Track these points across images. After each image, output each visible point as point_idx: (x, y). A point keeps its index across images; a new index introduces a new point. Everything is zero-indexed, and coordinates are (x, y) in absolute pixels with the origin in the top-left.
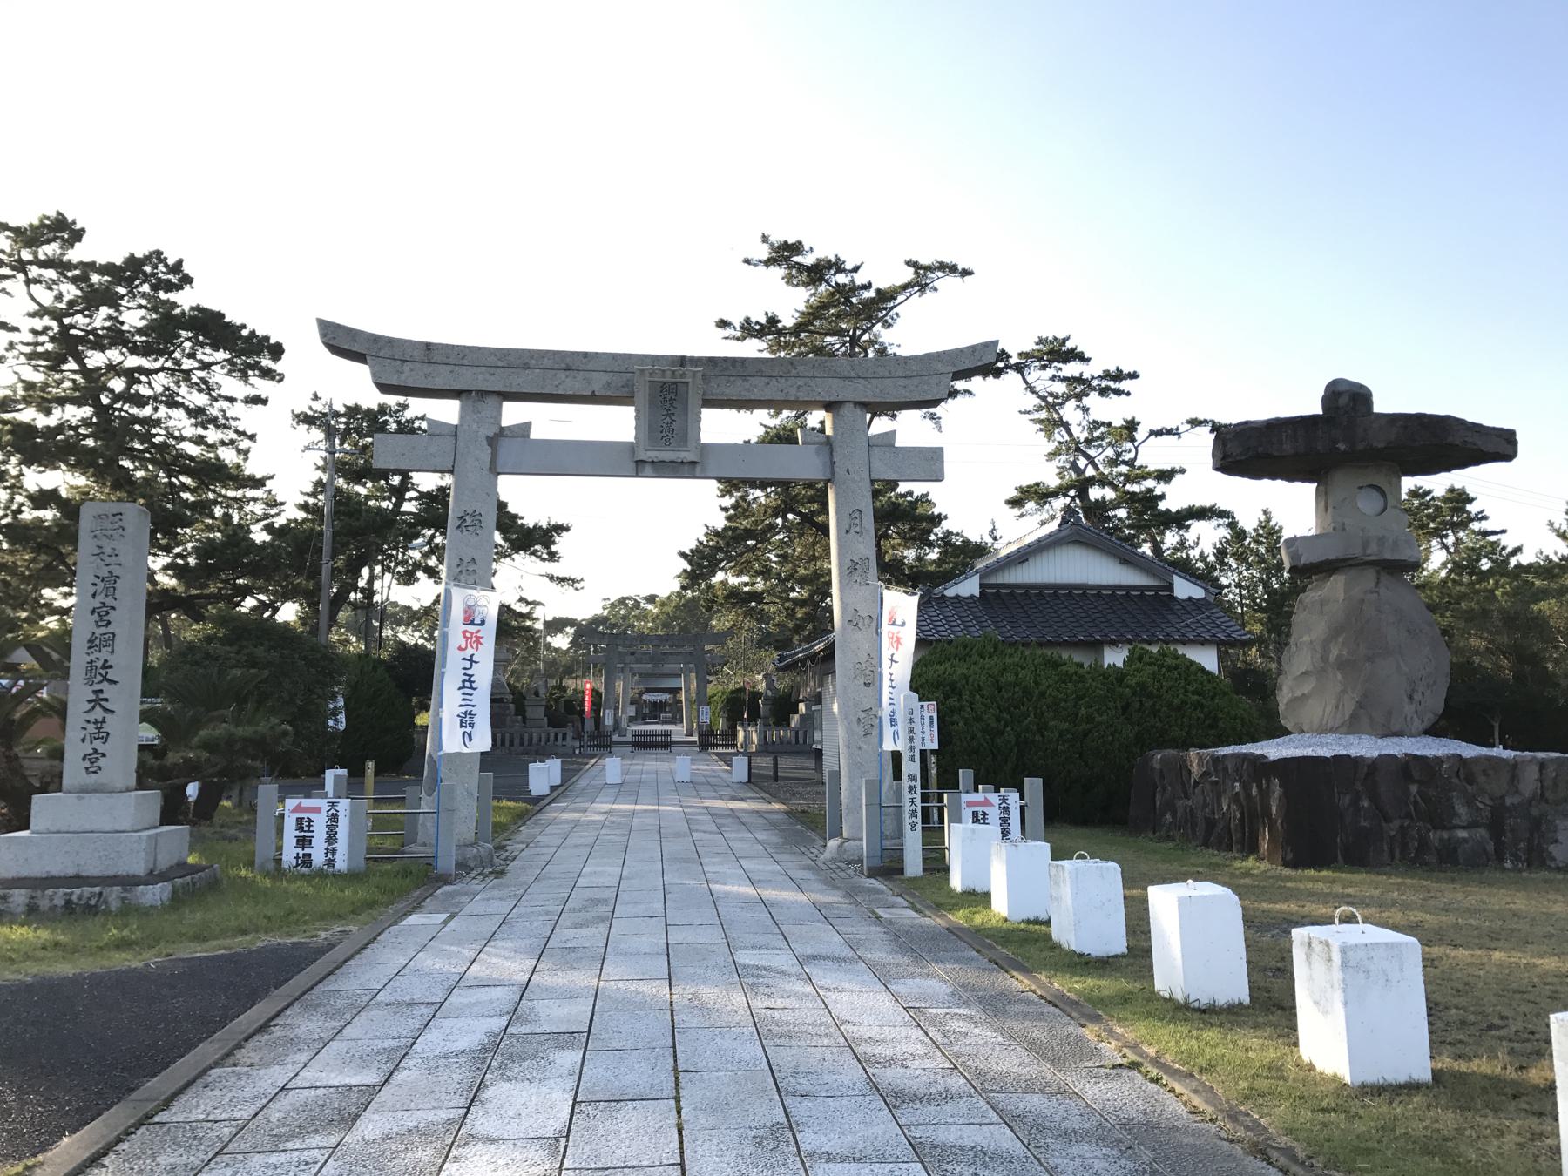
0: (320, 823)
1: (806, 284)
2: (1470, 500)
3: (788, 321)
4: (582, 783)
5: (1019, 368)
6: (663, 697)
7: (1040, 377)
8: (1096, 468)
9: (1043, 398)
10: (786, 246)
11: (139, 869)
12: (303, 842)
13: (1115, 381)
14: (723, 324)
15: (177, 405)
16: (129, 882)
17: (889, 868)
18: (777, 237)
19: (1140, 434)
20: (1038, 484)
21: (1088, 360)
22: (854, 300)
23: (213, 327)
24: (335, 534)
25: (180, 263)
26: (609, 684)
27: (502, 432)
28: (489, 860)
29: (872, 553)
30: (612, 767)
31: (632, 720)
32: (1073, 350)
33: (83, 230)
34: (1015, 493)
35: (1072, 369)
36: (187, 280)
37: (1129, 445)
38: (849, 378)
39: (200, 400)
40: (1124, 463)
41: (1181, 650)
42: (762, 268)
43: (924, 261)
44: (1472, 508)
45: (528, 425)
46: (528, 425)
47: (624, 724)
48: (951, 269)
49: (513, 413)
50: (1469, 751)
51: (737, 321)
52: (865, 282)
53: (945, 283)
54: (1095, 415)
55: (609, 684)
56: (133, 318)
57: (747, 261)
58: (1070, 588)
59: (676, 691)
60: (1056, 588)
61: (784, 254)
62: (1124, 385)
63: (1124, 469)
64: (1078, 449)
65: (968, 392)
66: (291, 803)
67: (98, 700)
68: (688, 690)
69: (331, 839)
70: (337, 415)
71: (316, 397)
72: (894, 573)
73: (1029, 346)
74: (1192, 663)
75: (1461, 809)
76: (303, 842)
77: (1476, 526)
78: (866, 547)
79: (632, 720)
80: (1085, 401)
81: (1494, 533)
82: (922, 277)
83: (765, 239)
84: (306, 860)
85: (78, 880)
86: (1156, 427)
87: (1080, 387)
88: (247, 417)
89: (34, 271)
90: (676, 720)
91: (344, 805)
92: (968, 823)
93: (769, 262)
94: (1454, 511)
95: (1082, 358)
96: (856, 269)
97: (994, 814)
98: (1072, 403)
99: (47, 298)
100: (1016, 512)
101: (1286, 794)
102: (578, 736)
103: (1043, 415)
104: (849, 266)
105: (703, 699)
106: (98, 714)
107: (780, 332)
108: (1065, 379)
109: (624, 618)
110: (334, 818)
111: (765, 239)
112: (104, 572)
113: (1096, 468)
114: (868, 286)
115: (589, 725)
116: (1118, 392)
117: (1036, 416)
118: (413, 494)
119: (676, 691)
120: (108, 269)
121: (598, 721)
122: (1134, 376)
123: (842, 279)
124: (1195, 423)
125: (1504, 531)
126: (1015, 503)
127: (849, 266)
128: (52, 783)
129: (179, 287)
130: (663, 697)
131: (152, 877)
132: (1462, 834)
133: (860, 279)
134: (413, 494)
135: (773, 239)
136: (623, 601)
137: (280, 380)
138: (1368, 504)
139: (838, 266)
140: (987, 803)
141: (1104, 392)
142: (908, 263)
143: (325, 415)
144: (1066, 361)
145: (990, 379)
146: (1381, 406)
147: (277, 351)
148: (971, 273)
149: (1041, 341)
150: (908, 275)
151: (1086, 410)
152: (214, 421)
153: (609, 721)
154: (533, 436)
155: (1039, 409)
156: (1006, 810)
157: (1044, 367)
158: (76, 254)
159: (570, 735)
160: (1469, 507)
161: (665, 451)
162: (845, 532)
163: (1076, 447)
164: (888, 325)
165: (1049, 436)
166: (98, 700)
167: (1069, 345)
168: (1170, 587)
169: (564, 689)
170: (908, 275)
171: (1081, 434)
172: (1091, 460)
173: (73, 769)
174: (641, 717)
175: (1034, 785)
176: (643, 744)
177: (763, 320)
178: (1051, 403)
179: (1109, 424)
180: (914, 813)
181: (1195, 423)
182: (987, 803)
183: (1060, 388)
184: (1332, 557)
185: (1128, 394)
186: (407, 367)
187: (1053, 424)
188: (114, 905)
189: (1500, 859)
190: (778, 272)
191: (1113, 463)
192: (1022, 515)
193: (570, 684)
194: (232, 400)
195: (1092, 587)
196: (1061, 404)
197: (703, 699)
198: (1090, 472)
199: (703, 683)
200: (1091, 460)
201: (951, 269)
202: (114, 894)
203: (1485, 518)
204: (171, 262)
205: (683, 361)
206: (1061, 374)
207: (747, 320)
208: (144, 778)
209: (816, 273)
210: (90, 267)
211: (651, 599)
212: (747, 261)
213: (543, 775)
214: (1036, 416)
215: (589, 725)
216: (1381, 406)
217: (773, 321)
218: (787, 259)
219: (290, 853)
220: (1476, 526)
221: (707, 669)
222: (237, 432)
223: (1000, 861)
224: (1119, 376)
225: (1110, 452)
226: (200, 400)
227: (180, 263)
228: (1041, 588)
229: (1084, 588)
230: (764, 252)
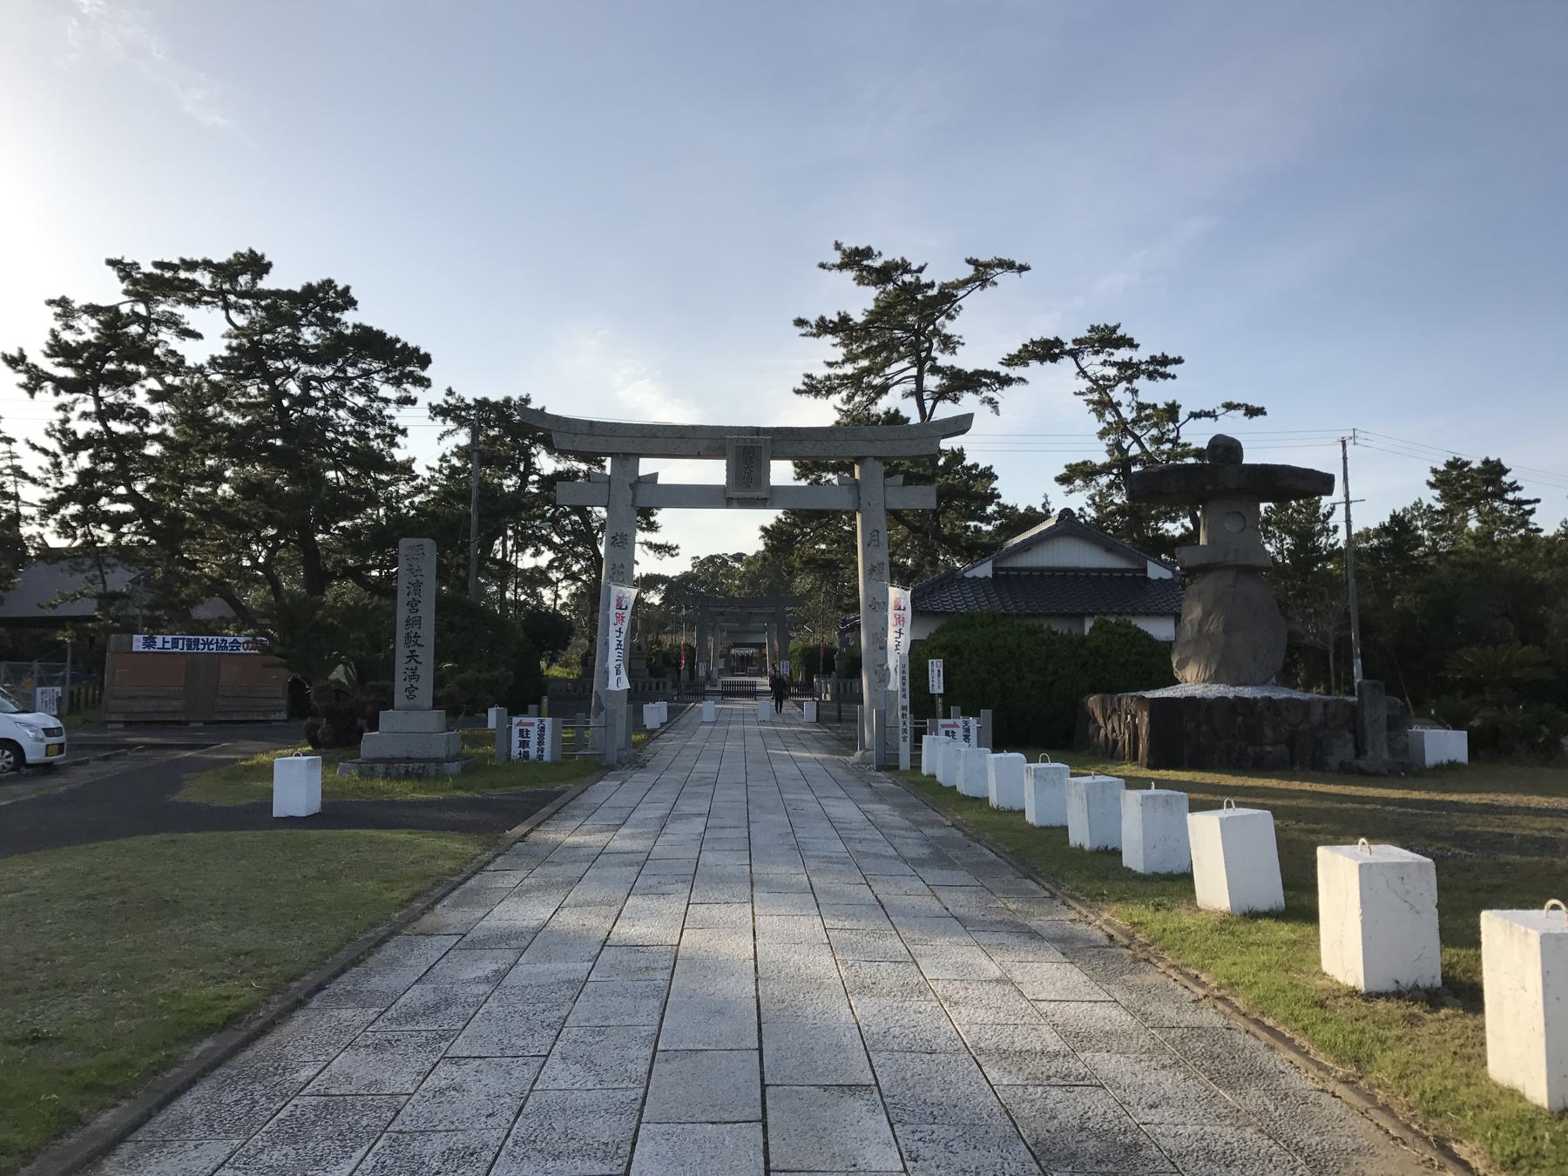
0: (535, 734)
1: (875, 284)
2: (1505, 472)
3: (858, 317)
4: (683, 721)
5: (1074, 354)
6: (751, 651)
7: (1093, 363)
8: (1142, 445)
9: (1095, 382)
10: (857, 252)
11: (443, 755)
12: (524, 744)
13: (1159, 367)
14: (800, 322)
15: (343, 405)
16: (439, 761)
17: (888, 764)
18: (849, 244)
19: (1182, 416)
20: (1085, 463)
21: (1137, 346)
22: (919, 297)
23: (373, 343)
24: (480, 517)
25: (347, 289)
26: (702, 640)
27: (640, 480)
28: (633, 759)
29: (886, 560)
30: (708, 708)
31: (721, 672)
32: (1122, 338)
33: (270, 265)
34: (1064, 471)
35: (1122, 354)
36: (352, 303)
37: (1171, 426)
38: (870, 441)
39: (361, 401)
40: (1169, 440)
41: (1134, 622)
42: (835, 272)
43: (982, 259)
44: (1507, 479)
45: (655, 475)
46: (655, 475)
47: (715, 675)
48: (1009, 265)
49: (646, 466)
50: (1281, 694)
51: (813, 320)
52: (928, 281)
53: (1004, 278)
54: (1143, 398)
55: (702, 640)
56: (309, 335)
57: (822, 266)
58: (1065, 570)
59: (761, 646)
60: (1053, 570)
61: (855, 259)
62: (1170, 369)
63: (1167, 446)
64: (1126, 429)
65: (1021, 380)
66: (516, 720)
67: (412, 656)
68: (771, 646)
69: (541, 743)
70: (468, 407)
71: (450, 392)
72: (901, 576)
73: (1083, 333)
74: (1140, 631)
75: (1268, 732)
76: (524, 744)
77: (1510, 496)
78: (882, 556)
79: (721, 672)
80: (1136, 383)
81: (1528, 502)
82: (982, 274)
83: (838, 246)
84: (526, 755)
85: (409, 760)
86: (1197, 410)
87: (1129, 371)
88: (402, 417)
89: (232, 298)
90: (761, 673)
91: (548, 721)
92: (942, 737)
93: (841, 267)
94: (1488, 482)
95: (1131, 344)
96: (921, 270)
97: (960, 732)
98: (1124, 384)
99: (241, 320)
100: (1065, 488)
101: (1151, 722)
102: (675, 686)
103: (1096, 396)
104: (914, 267)
105: (784, 654)
106: (413, 664)
107: (852, 329)
108: (1114, 364)
109: (714, 575)
110: (542, 729)
111: (838, 246)
112: (413, 580)
113: (1142, 445)
114: (931, 285)
115: (685, 675)
116: (1165, 376)
117: (1090, 397)
118: (534, 478)
119: (761, 646)
120: (290, 295)
121: (692, 673)
122: (1179, 361)
123: (908, 278)
124: (1229, 406)
125: (1538, 501)
126: (1062, 480)
127: (914, 267)
128: (389, 704)
129: (344, 309)
130: (751, 651)
131: (450, 759)
132: (1269, 749)
133: (925, 278)
134: (534, 478)
135: (845, 246)
136: (711, 559)
137: (429, 386)
138: (1232, 526)
139: (904, 267)
140: (955, 725)
141: (1151, 376)
142: (969, 262)
143: (458, 408)
144: (1117, 347)
145: (1048, 364)
146: (1249, 459)
147: (425, 361)
148: (1027, 269)
149: (1093, 329)
150: (969, 271)
151: (1135, 392)
152: (373, 418)
153: (702, 673)
154: (660, 481)
155: (1091, 391)
156: (968, 730)
157: (1097, 353)
158: (265, 284)
159: (669, 686)
160: (1504, 479)
161: (745, 488)
162: (867, 545)
163: (1122, 427)
164: (951, 318)
165: (1101, 415)
166: (412, 656)
167: (1120, 332)
168: (1145, 570)
169: (659, 644)
170: (969, 271)
171: (1128, 414)
172: (1137, 439)
173: (400, 698)
174: (731, 671)
175: (987, 714)
176: (730, 693)
177: (836, 319)
178: (1101, 386)
179: (1155, 406)
180: (905, 731)
181: (1229, 406)
182: (955, 725)
183: (1112, 372)
184: (1205, 561)
185: (1174, 377)
186: (577, 439)
187: (1103, 405)
188: (433, 773)
189: (1293, 764)
190: (849, 275)
191: (1157, 441)
192: (1071, 492)
193: (667, 640)
194: (386, 401)
195: (1094, 570)
196: (1112, 387)
197: (784, 654)
198: (1135, 450)
199: (785, 639)
200: (1137, 439)
201: (1009, 265)
202: (432, 767)
203: (1519, 489)
204: (339, 288)
205: (758, 431)
206: (1112, 359)
207: (822, 319)
208: (437, 704)
209: (883, 275)
210: (277, 294)
211: (738, 557)
212: (822, 266)
213: (654, 713)
214: (1090, 397)
215: (685, 675)
216: (1249, 459)
217: (845, 319)
218: (858, 264)
219: (516, 750)
220: (1510, 496)
221: (784, 629)
222: (391, 427)
223: (959, 757)
224: (1165, 361)
225: (1154, 432)
226: (361, 401)
227: (347, 289)
228: (1042, 570)
229: (1076, 570)
230: (837, 258)
